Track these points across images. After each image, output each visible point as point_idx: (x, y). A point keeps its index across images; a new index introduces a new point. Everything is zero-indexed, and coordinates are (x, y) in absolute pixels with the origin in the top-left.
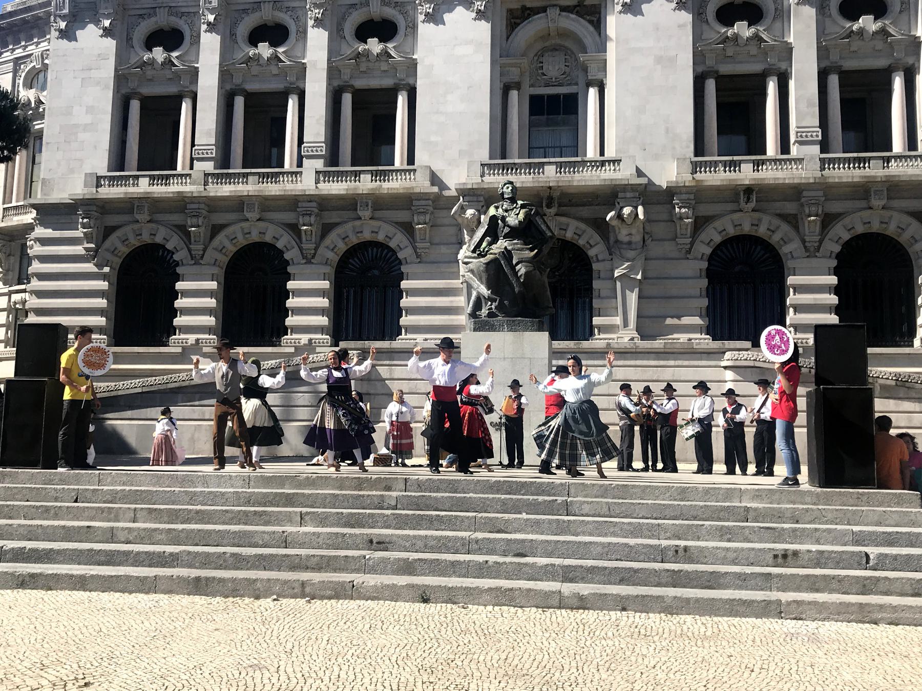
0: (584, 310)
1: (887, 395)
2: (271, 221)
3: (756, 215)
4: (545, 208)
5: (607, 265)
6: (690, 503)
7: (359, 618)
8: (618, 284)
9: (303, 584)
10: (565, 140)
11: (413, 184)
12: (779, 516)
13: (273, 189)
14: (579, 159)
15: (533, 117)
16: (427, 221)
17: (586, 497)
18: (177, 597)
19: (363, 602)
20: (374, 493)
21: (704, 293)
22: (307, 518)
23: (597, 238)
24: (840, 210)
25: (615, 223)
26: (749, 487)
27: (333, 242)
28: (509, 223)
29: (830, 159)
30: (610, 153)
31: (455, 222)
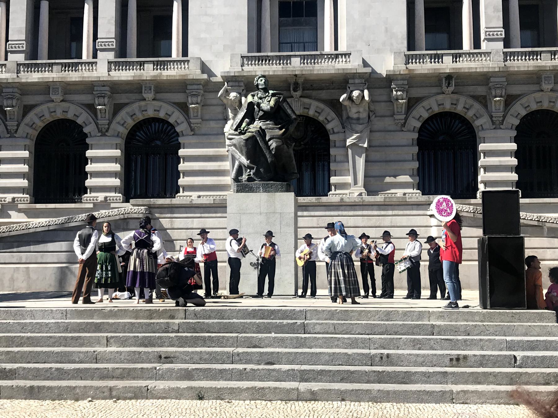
0: (323, 171)
1: (553, 235)
2: (72, 102)
3: (455, 96)
4: (292, 92)
5: (341, 136)
6: (392, 322)
7: (153, 412)
8: (350, 151)
9: (111, 389)
10: (308, 37)
11: (187, 72)
12: (456, 331)
13: (73, 76)
14: (318, 53)
15: (282, 19)
16: (199, 101)
17: (318, 320)
18: (17, 401)
19: (155, 400)
20: (162, 321)
21: (415, 157)
22: (112, 341)
23: (333, 115)
24: (519, 93)
25: (347, 103)
26: (435, 310)
27: (122, 119)
28: (263, 108)
29: (511, 52)
30: (342, 48)
31: (220, 102)
